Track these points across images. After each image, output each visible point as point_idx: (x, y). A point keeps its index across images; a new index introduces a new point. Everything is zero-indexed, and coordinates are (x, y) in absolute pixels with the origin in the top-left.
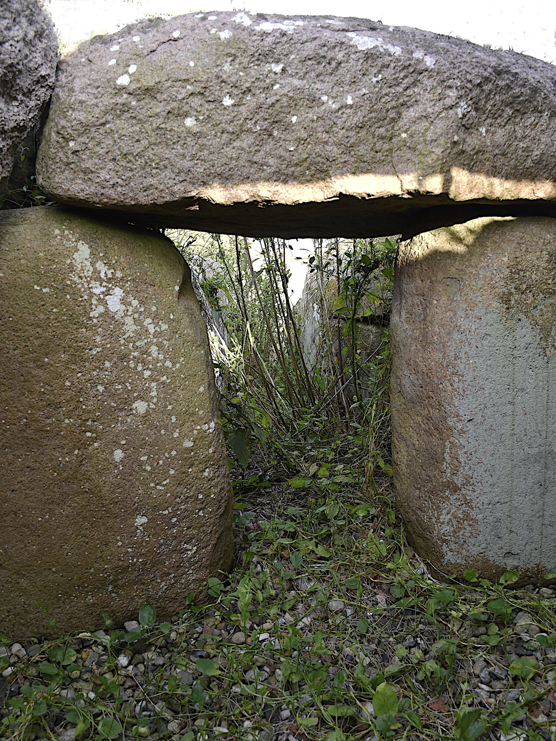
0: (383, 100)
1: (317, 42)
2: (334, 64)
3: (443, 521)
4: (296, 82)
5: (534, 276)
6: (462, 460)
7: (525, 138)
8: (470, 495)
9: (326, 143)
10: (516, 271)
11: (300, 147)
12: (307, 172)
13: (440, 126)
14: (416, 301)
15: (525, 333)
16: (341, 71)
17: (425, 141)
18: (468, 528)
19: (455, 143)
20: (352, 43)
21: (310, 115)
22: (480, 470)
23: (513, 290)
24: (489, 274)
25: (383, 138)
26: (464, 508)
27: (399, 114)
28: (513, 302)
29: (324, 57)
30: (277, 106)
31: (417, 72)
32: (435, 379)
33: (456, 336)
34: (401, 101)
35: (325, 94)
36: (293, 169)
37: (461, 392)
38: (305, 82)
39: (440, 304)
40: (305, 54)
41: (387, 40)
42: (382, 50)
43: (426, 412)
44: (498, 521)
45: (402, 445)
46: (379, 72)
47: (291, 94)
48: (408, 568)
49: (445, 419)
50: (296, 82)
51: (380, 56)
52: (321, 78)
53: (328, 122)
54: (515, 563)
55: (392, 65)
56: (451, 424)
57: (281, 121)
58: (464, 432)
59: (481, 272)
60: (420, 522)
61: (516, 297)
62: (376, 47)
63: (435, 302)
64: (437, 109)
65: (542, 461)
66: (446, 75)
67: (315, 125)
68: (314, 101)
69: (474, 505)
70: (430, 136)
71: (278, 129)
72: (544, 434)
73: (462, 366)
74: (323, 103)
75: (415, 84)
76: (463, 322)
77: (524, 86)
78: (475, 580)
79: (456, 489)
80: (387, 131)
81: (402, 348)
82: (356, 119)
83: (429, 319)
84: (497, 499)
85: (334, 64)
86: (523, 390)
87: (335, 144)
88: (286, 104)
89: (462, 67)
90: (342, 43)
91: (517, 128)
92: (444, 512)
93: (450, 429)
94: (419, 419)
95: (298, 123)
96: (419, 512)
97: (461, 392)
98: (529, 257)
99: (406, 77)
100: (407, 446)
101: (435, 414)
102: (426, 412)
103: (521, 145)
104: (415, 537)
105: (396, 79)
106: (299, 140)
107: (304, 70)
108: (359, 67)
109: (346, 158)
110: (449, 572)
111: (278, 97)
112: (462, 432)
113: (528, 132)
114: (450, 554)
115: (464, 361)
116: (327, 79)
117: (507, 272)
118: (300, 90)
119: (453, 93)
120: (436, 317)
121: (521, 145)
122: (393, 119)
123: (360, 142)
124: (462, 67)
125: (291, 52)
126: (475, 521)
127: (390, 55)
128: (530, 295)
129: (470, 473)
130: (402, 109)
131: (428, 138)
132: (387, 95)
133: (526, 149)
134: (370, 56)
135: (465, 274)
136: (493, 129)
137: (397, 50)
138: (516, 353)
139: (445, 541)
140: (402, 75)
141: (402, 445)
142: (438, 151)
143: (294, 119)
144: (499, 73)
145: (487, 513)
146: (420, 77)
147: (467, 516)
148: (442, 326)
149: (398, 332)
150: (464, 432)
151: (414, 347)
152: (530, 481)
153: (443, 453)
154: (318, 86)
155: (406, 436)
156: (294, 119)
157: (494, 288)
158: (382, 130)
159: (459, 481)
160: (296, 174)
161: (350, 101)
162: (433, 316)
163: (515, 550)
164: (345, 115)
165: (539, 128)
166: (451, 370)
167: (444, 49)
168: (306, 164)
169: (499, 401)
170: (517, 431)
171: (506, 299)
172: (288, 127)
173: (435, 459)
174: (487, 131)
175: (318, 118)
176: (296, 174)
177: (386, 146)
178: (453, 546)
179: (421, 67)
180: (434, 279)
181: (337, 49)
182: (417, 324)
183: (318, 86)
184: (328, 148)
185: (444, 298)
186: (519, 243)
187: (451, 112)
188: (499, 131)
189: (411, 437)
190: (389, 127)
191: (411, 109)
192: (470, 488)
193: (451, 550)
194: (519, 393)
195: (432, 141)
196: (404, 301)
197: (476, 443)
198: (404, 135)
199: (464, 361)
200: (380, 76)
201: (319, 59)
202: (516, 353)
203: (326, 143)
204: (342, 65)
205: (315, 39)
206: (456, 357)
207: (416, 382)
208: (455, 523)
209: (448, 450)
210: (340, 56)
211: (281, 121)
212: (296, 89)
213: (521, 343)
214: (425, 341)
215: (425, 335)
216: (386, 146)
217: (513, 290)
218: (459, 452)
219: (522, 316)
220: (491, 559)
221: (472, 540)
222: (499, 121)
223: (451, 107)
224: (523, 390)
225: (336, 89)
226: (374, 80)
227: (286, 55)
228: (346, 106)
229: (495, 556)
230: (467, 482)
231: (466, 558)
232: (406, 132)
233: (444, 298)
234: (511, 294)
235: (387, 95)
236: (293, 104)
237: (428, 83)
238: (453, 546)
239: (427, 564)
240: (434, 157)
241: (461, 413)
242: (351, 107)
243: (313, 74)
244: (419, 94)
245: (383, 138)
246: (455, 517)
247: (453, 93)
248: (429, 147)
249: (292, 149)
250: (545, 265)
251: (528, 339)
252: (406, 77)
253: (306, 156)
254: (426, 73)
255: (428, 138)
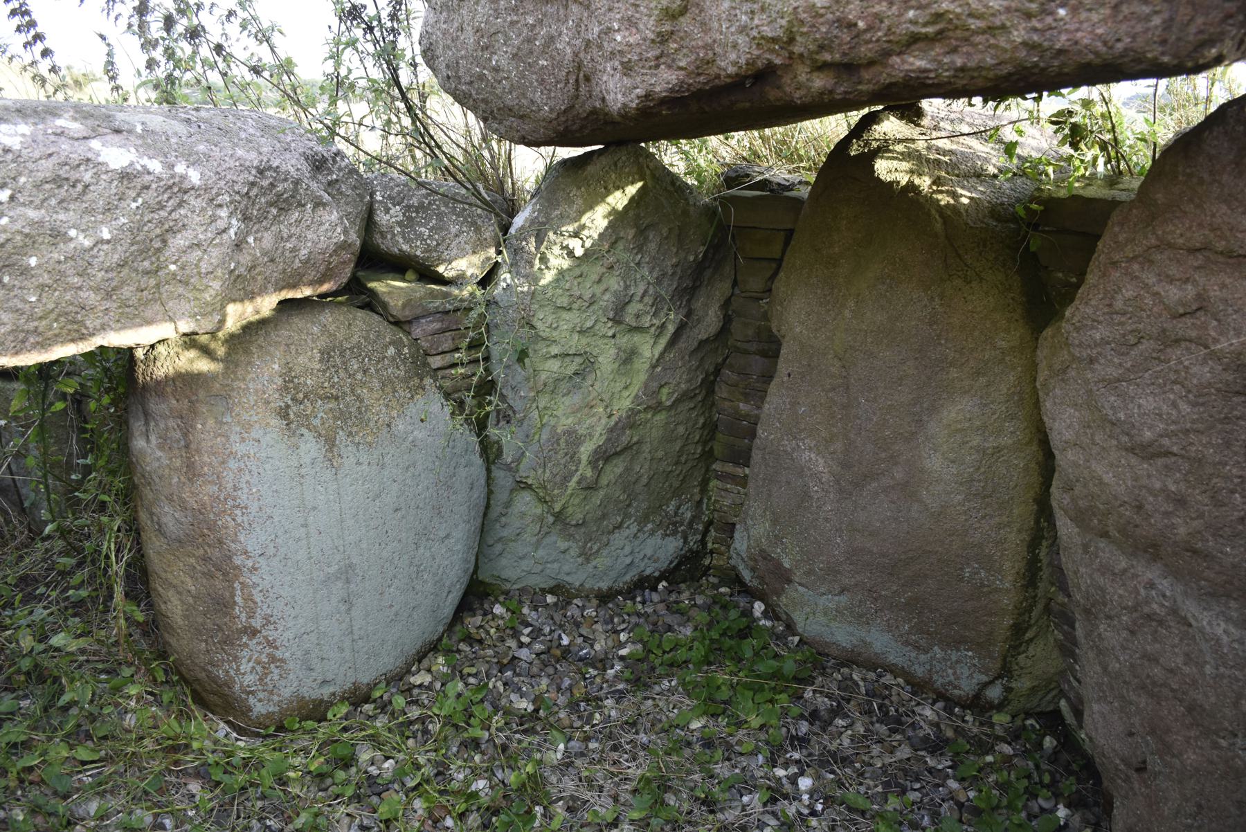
0: (146, 228)
1: (54, 160)
2: (80, 187)
3: (244, 671)
4: (32, 214)
5: (309, 382)
6: (258, 600)
7: (290, 237)
8: (271, 633)
9: (80, 288)
10: (289, 382)
11: (44, 295)
12: (55, 325)
13: (215, 253)
14: (172, 423)
15: (310, 447)
16: (89, 196)
17: (199, 273)
18: (276, 671)
19: (232, 271)
20: (101, 159)
21: (56, 256)
22: (280, 605)
23: (290, 402)
24: (260, 386)
25: (148, 273)
26: (267, 650)
27: (164, 241)
28: (292, 416)
29: (67, 179)
30: (9, 247)
31: (178, 189)
32: (212, 516)
33: (232, 464)
34: (166, 227)
35: (74, 227)
36: (36, 324)
37: (246, 525)
38: (43, 211)
39: (205, 428)
40: (40, 176)
41: (141, 150)
42: (139, 168)
43: (201, 552)
44: (307, 652)
45: (171, 593)
46: (138, 195)
47: (27, 231)
48: (210, 734)
49: (230, 558)
50: (32, 214)
51: (138, 175)
52: (65, 205)
53: (80, 262)
54: (332, 690)
55: (154, 186)
56: (239, 562)
57: (14, 265)
58: (256, 569)
59: (251, 385)
60: (215, 680)
61: (294, 408)
62: (132, 164)
63: (199, 426)
64: (209, 235)
65: (343, 577)
66: (214, 192)
67: (63, 267)
68: (58, 235)
69: (278, 644)
70: (204, 267)
71: (10, 275)
72: (341, 549)
73: (244, 497)
74: (72, 239)
75: (180, 205)
76: (239, 448)
77: (286, 180)
78: (297, 726)
79: (254, 633)
80: (152, 263)
81: (157, 480)
82: (116, 257)
83: (193, 446)
84: (303, 630)
85: (80, 187)
86: (314, 508)
87: (91, 288)
88: (21, 244)
89: (229, 177)
90: (88, 160)
91: (282, 227)
92: (244, 661)
93: (237, 567)
94: (192, 560)
95: (39, 266)
96: (209, 667)
97: (246, 525)
98: (301, 360)
99: (170, 198)
100: (180, 593)
101: (215, 554)
102: (201, 552)
103: (289, 245)
104: (212, 697)
105: (159, 202)
106: (42, 287)
107: (41, 197)
108: (114, 191)
109: (108, 304)
110: (260, 725)
111: (9, 235)
112: (254, 569)
113: (293, 230)
114: (259, 704)
115: (246, 491)
116: (72, 206)
117: (280, 381)
118: (40, 223)
119: (223, 213)
120: (203, 444)
121: (289, 245)
122: (158, 250)
123: (123, 283)
124: (229, 177)
125: (20, 174)
126: (282, 660)
127: (149, 173)
128: (308, 404)
129: (269, 612)
130: (168, 236)
131: (203, 271)
132: (149, 222)
133: (294, 250)
134: (126, 176)
135: (233, 390)
136: (259, 235)
137: (155, 166)
138: (303, 471)
139: (252, 693)
140: (166, 196)
141: (171, 593)
142: (216, 285)
143: (33, 261)
144: (261, 172)
145: (295, 648)
146: (186, 197)
147: (273, 659)
148: (214, 454)
149: (148, 460)
150: (256, 569)
151: (175, 480)
152: (334, 600)
153: (233, 596)
154: (62, 216)
155: (175, 582)
156: (33, 261)
157: (269, 403)
158: (146, 264)
159: (257, 623)
160: (41, 329)
161: (106, 235)
162: (199, 443)
163: (330, 677)
164: (102, 253)
165: (304, 225)
166: (230, 503)
167: (204, 154)
168: (53, 316)
169: (291, 526)
170: (314, 553)
171: (283, 413)
172: (25, 271)
173: (224, 605)
174: (255, 239)
175: (66, 258)
176: (41, 329)
177: (152, 282)
178: (261, 695)
179: (186, 185)
180: (194, 398)
181: (82, 168)
182: (176, 452)
183: (62, 216)
184: (81, 294)
185: (211, 422)
186: (287, 345)
187: (225, 236)
188: (266, 235)
189: (183, 582)
190: (154, 259)
191: (179, 236)
192: (272, 627)
193: (260, 700)
194: (312, 513)
195: (207, 273)
196: (152, 424)
197: (272, 578)
198: (173, 267)
199: (246, 491)
200: (140, 200)
201: (58, 181)
202: (303, 471)
203: (80, 288)
204: (91, 188)
205: (50, 155)
206: (235, 488)
207: (183, 520)
208: (259, 668)
209: (238, 592)
210: (87, 177)
211: (14, 265)
212: (32, 223)
213: (306, 460)
214: (191, 471)
215: (190, 466)
216: (152, 282)
217: (290, 402)
218: (254, 592)
219: (304, 431)
220: (306, 695)
221: (283, 682)
222: (264, 224)
223: (224, 231)
224: (314, 508)
225: (86, 218)
226: (134, 205)
227: (14, 179)
228: (102, 241)
229: (312, 691)
230: (268, 620)
231: (279, 704)
232: (174, 263)
233: (211, 422)
234: (288, 406)
235: (149, 222)
236: (30, 242)
237: (197, 203)
238: (261, 695)
239: (228, 722)
240: (213, 293)
241: (249, 549)
242: (108, 242)
243: (53, 202)
244: (186, 217)
245: (148, 273)
246: (259, 663)
247: (223, 213)
248: (205, 281)
249: (33, 299)
250: (318, 367)
251: (314, 454)
252: (170, 198)
253: (53, 306)
254: (192, 192)
255: (203, 271)
